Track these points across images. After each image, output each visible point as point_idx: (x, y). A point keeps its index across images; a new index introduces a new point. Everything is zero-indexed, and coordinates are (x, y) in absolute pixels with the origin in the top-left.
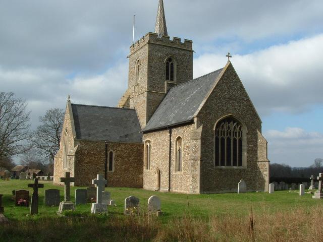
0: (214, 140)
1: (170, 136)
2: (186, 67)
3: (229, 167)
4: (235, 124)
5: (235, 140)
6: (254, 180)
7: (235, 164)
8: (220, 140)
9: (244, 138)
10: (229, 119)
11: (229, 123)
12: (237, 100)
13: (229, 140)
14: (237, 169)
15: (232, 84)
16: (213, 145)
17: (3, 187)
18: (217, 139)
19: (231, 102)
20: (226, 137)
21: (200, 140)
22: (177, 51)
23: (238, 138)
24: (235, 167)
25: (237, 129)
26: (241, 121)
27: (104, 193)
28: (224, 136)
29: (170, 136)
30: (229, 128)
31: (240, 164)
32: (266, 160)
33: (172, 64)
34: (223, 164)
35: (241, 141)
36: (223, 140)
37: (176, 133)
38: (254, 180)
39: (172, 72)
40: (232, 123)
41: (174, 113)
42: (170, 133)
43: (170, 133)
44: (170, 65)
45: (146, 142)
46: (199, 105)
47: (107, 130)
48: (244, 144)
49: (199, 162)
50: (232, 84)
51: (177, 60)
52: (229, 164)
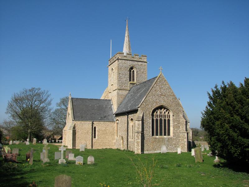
0: (151, 120)
1: (128, 118)
2: (143, 72)
3: (161, 137)
4: (165, 110)
5: (165, 120)
6: (178, 144)
7: (165, 135)
8: (167, 120)
9: (171, 119)
10: (161, 107)
11: (161, 110)
12: (166, 96)
13: (165, 120)
14: (166, 138)
15: (162, 86)
16: (150, 123)
17: (1, 159)
18: (153, 120)
19: (162, 97)
20: (159, 119)
21: (141, 121)
22: (136, 63)
23: (167, 119)
24: (165, 137)
25: (167, 113)
26: (169, 108)
27: (216, 136)
28: (162, 117)
29: (128, 118)
30: (161, 113)
31: (169, 134)
32: (185, 132)
33: (133, 71)
34: (157, 135)
35: (169, 121)
36: (157, 120)
37: (131, 116)
38: (178, 144)
39: (133, 76)
40: (163, 109)
41: (221, 94)
42: (128, 116)
43: (128, 116)
44: (132, 72)
45: (117, 120)
46: (142, 100)
47: (93, 113)
48: (171, 122)
49: (140, 134)
50: (162, 86)
51: (136, 69)
52: (161, 134)
